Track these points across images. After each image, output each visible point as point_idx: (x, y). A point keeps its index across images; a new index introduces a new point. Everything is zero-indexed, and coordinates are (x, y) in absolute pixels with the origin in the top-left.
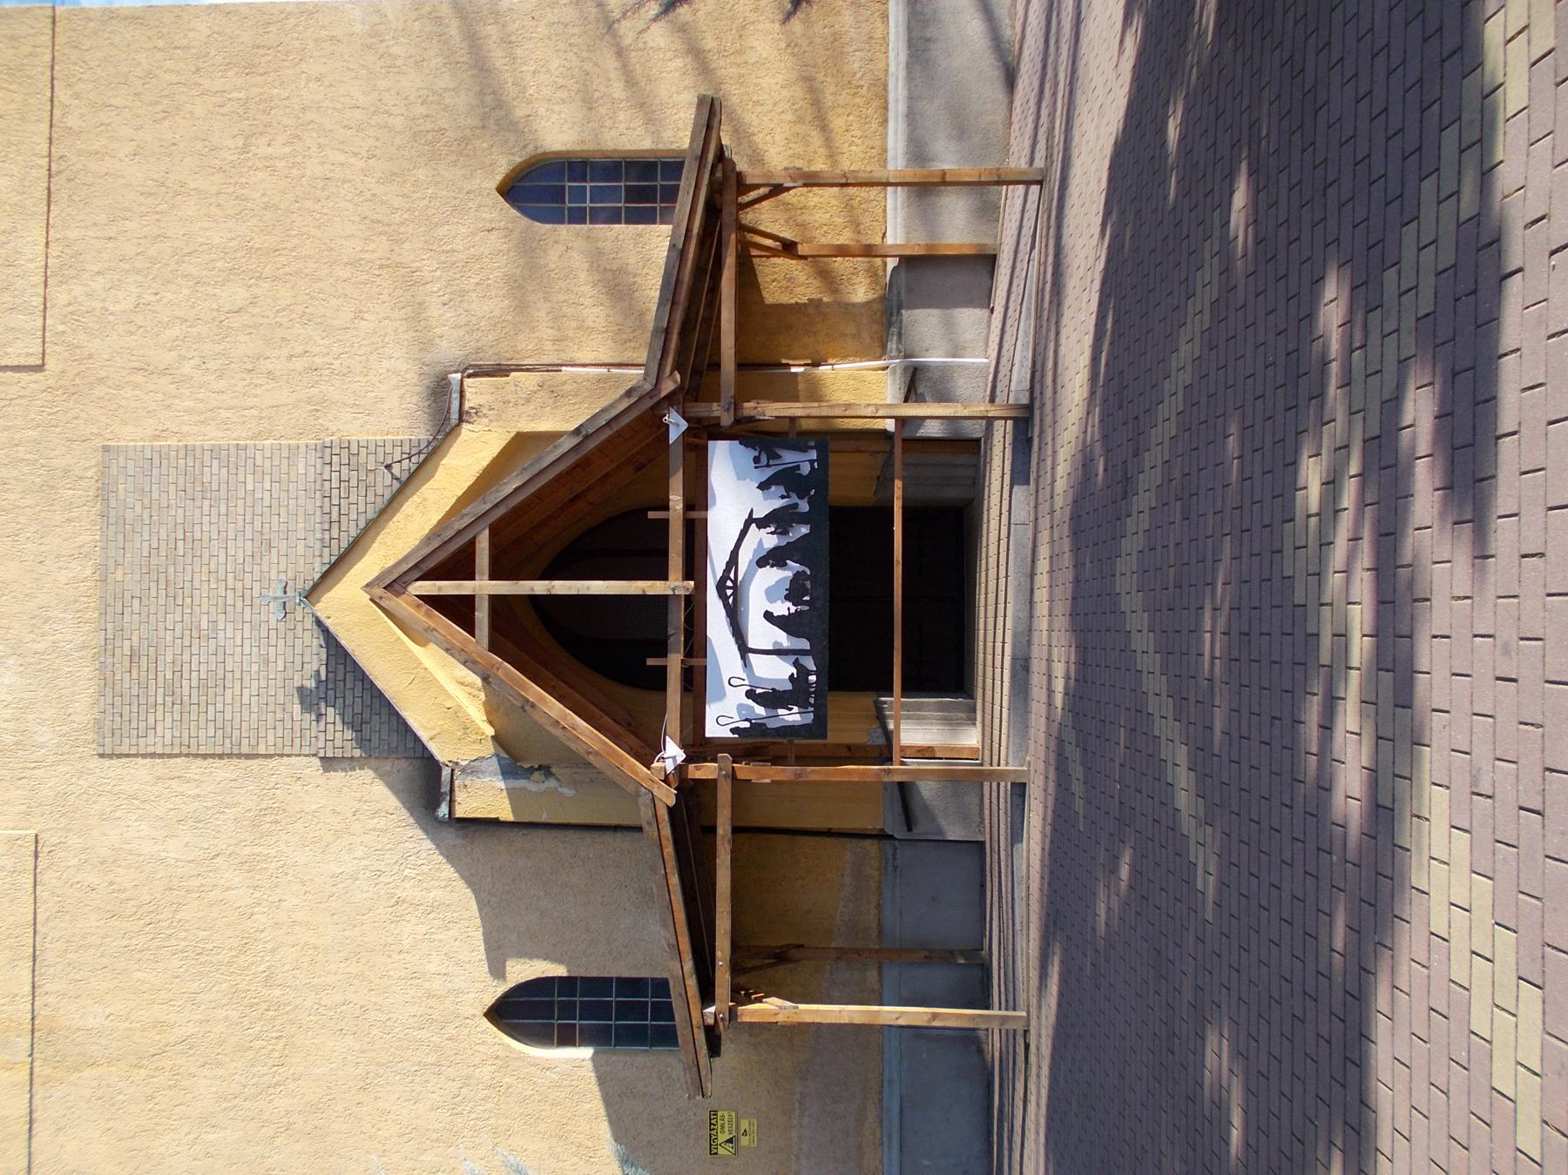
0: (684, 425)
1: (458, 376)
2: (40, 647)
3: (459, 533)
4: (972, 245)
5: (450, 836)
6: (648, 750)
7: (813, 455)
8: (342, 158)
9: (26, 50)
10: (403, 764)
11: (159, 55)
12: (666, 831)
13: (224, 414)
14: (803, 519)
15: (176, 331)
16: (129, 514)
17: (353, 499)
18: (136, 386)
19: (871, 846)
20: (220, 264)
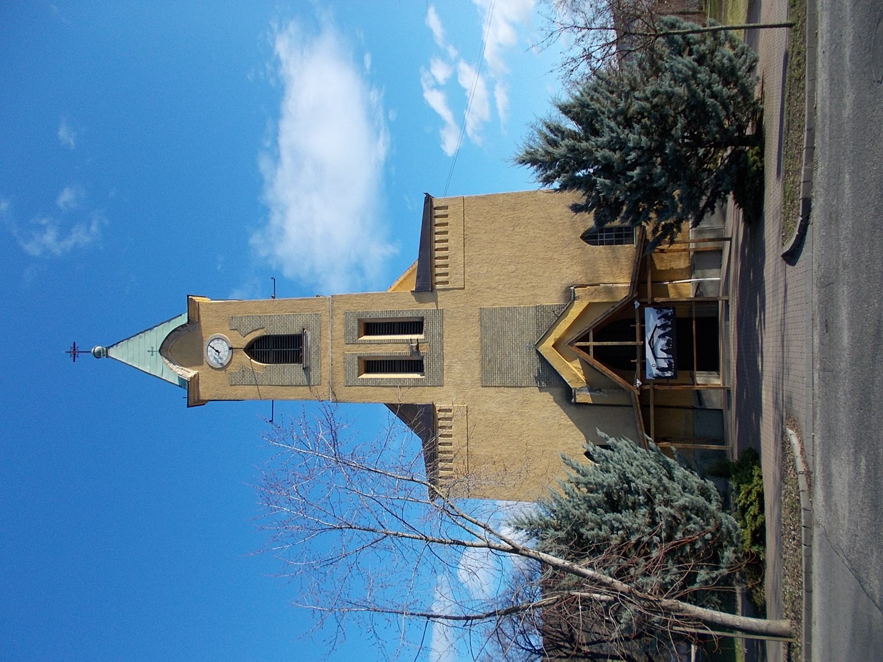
0: (639, 304)
1: (573, 288)
2: (466, 359)
3: (585, 331)
4: (714, 247)
5: (573, 408)
6: (633, 383)
7: (672, 310)
8: (539, 231)
9: (457, 208)
10: (560, 389)
11: (490, 207)
12: (638, 401)
13: (510, 299)
14: (669, 326)
15: (497, 278)
16: (487, 325)
17: (545, 320)
18: (487, 292)
19: (690, 411)
20: (508, 260)
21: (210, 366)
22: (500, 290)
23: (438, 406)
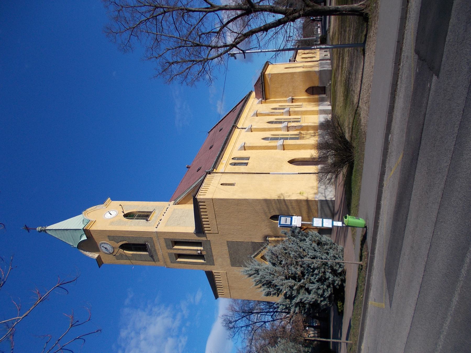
15: (233, 230)
21: (105, 253)
22: (235, 235)
23: (214, 271)
